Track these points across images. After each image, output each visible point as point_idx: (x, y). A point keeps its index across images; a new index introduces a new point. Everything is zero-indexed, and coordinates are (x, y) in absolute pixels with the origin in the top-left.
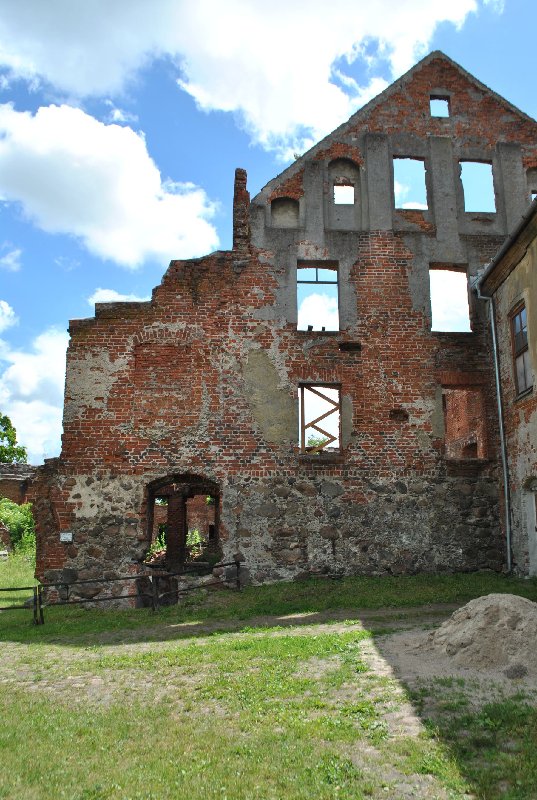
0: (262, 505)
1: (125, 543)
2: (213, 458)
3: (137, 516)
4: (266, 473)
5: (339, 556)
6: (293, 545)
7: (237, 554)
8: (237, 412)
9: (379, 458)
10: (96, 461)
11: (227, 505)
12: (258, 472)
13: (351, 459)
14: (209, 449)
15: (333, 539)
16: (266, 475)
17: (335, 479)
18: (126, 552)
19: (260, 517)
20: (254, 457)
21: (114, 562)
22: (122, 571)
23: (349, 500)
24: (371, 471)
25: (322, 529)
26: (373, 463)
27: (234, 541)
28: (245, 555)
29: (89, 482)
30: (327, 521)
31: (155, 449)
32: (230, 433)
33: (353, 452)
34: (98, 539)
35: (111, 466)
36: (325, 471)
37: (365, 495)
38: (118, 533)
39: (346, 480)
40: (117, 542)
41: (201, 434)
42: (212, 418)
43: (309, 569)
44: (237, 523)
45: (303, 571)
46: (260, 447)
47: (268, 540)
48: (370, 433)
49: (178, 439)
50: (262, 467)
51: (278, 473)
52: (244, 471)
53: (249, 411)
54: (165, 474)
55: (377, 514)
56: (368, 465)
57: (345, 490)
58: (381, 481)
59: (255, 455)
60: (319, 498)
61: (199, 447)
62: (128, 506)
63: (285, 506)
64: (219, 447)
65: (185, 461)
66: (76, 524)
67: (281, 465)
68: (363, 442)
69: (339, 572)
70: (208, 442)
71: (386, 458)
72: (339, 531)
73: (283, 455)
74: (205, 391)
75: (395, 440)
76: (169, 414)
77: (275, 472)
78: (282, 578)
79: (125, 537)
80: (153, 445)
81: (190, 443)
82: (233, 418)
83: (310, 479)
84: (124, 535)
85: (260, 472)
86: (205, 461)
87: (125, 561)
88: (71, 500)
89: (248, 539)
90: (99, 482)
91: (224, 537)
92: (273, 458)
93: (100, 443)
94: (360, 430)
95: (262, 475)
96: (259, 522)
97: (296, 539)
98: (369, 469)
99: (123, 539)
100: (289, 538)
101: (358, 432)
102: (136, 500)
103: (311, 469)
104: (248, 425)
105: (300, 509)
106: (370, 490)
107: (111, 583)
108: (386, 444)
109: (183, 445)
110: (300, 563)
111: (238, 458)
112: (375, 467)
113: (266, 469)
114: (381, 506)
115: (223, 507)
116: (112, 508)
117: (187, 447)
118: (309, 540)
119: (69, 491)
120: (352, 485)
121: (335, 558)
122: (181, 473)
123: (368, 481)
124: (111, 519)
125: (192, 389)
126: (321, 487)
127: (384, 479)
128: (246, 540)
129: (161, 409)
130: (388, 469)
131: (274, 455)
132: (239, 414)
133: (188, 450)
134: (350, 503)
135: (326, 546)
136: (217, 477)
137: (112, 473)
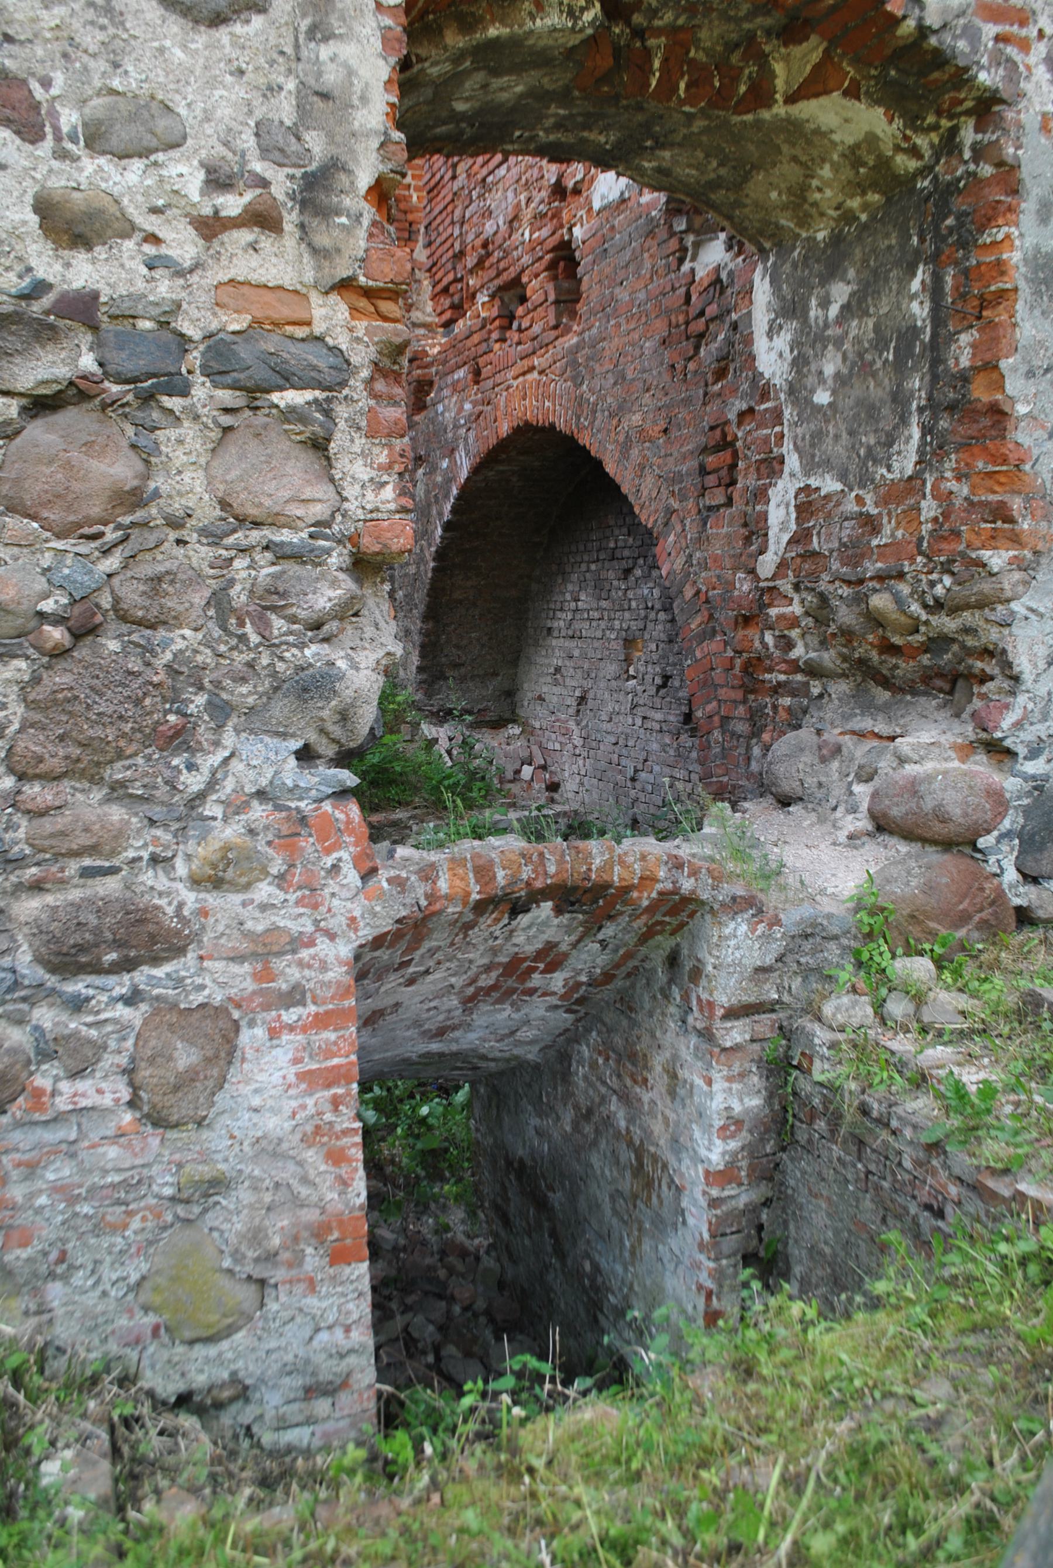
1: (219, 600)
3: (330, 315)
18: (244, 693)
21: (118, 791)
22: (213, 880)
40: (132, 594)
62: (232, 204)
79: (213, 536)
84: (208, 513)
87: (242, 776)
91: (1015, 540)
99: (201, 554)
102: (316, 143)
107: (105, 992)
115: (1025, 290)
124: (44, 333)
136: (990, 30)
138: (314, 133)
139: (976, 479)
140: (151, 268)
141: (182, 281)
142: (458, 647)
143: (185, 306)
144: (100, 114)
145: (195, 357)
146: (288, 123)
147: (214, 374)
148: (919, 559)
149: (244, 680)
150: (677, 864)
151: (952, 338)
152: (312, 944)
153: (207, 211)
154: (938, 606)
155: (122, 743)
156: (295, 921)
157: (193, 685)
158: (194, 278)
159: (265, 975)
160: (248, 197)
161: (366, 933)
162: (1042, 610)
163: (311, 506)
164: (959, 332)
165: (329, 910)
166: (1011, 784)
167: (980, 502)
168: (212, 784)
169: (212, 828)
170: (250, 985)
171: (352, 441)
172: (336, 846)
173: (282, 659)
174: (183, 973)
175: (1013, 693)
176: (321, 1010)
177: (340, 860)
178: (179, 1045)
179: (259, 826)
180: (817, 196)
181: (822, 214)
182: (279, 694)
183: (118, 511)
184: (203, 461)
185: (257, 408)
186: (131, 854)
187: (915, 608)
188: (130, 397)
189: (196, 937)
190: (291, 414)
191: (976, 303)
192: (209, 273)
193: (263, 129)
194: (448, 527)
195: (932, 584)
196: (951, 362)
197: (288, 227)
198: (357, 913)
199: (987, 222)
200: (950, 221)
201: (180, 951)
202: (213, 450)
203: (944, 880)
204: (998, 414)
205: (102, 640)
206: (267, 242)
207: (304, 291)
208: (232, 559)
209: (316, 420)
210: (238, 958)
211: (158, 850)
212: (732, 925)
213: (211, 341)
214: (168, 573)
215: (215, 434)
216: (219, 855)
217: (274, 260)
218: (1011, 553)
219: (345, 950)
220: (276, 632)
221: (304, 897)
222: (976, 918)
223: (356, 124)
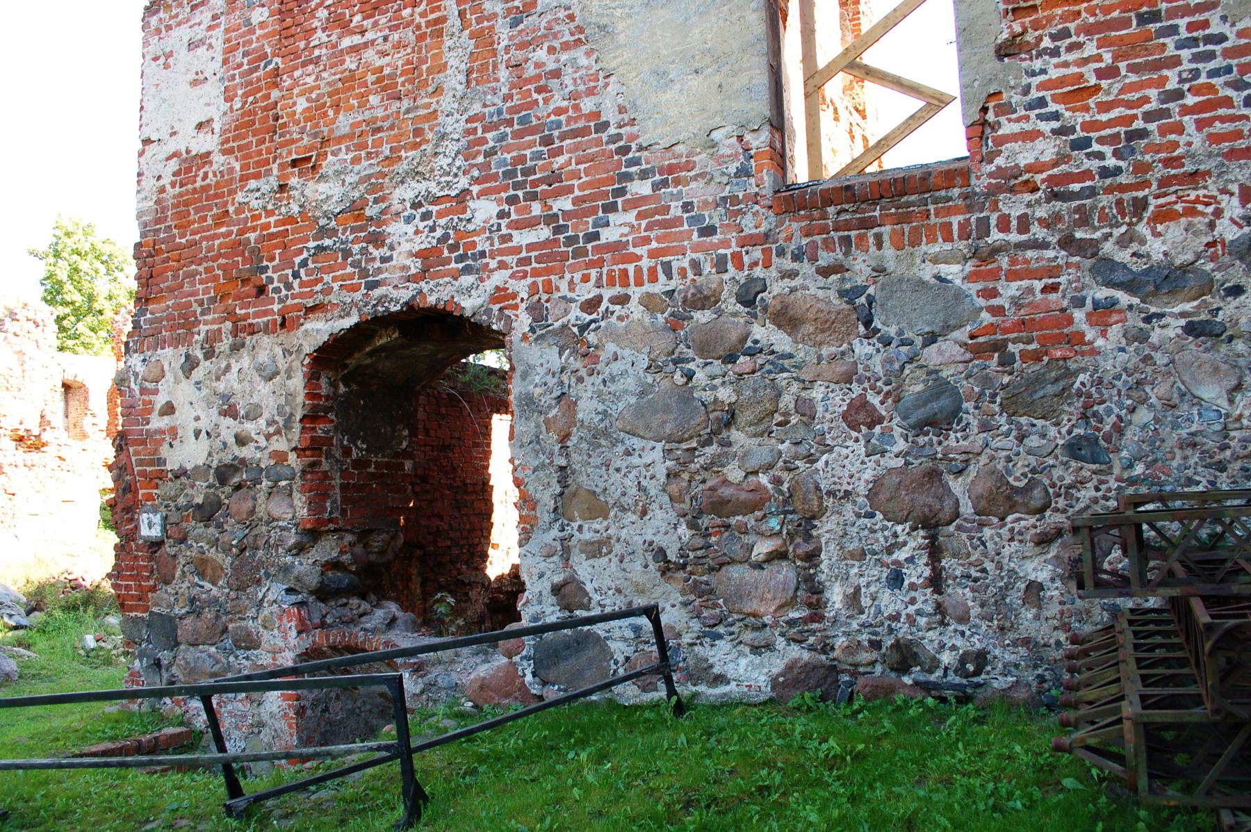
0: (642, 394)
2: (482, 244)
3: (292, 457)
4: (652, 271)
5: (960, 594)
6: (763, 548)
7: (565, 584)
8: (551, 66)
9: (1142, 134)
10: (201, 303)
12: (625, 273)
13: (1000, 161)
14: (468, 215)
15: (930, 524)
16: (653, 278)
17: (941, 263)
18: (272, 570)
19: (636, 442)
20: (612, 217)
23: (999, 347)
24: (1105, 200)
25: (877, 482)
26: (1111, 162)
27: (555, 532)
28: (589, 587)
29: (190, 365)
30: (901, 445)
31: (327, 242)
32: (531, 145)
33: (1007, 128)
34: (211, 530)
35: (231, 315)
36: (886, 230)
37: (1079, 315)
38: (252, 512)
39: (984, 256)
41: (446, 168)
42: (477, 108)
43: (826, 648)
44: (562, 468)
45: (806, 656)
46: (628, 177)
47: (666, 528)
48: (1089, 30)
49: (382, 199)
50: (638, 251)
51: (696, 265)
52: (578, 276)
53: (588, 54)
54: (353, 320)
55: (1144, 401)
56: (1087, 175)
57: (981, 302)
58: (1163, 244)
59: (611, 208)
60: (862, 348)
61: (440, 214)
63: (725, 394)
64: (499, 202)
65: (405, 268)
66: (168, 488)
67: (709, 231)
68: (1054, 74)
69: (961, 669)
70: (465, 192)
71: (1179, 129)
72: (957, 486)
73: (711, 192)
74: (454, 21)
75: (1222, 38)
76: (359, 124)
77: (685, 263)
78: (721, 679)
80: (323, 232)
81: (416, 205)
82: (539, 90)
83: (825, 272)
85: (631, 268)
86: (460, 259)
88: (157, 422)
89: (598, 524)
90: (208, 363)
92: (676, 210)
93: (210, 249)
94: (1036, 26)
95: (639, 283)
96: (635, 460)
97: (774, 523)
98: (1092, 192)
100: (750, 520)
101: (1030, 37)
102: (288, 409)
103: (824, 230)
104: (587, 105)
105: (787, 401)
106: (1102, 293)
108: (1175, 62)
109: (398, 214)
110: (791, 623)
111: (558, 230)
112: (1123, 179)
113: (653, 254)
114: (1160, 359)
116: (236, 436)
117: (409, 220)
118: (826, 528)
119: (152, 397)
120: (1013, 276)
121: (939, 608)
122: (393, 309)
123: (1088, 249)
125: (419, 27)
126: (871, 299)
127: (1174, 231)
128: (590, 530)
129: (341, 117)
130: (1194, 178)
131: (679, 196)
132: (556, 74)
133: (410, 229)
134: (1007, 361)
135: (901, 555)
136: (496, 307)
137: (235, 333)
161: (298, 651)
168: (264, 597)
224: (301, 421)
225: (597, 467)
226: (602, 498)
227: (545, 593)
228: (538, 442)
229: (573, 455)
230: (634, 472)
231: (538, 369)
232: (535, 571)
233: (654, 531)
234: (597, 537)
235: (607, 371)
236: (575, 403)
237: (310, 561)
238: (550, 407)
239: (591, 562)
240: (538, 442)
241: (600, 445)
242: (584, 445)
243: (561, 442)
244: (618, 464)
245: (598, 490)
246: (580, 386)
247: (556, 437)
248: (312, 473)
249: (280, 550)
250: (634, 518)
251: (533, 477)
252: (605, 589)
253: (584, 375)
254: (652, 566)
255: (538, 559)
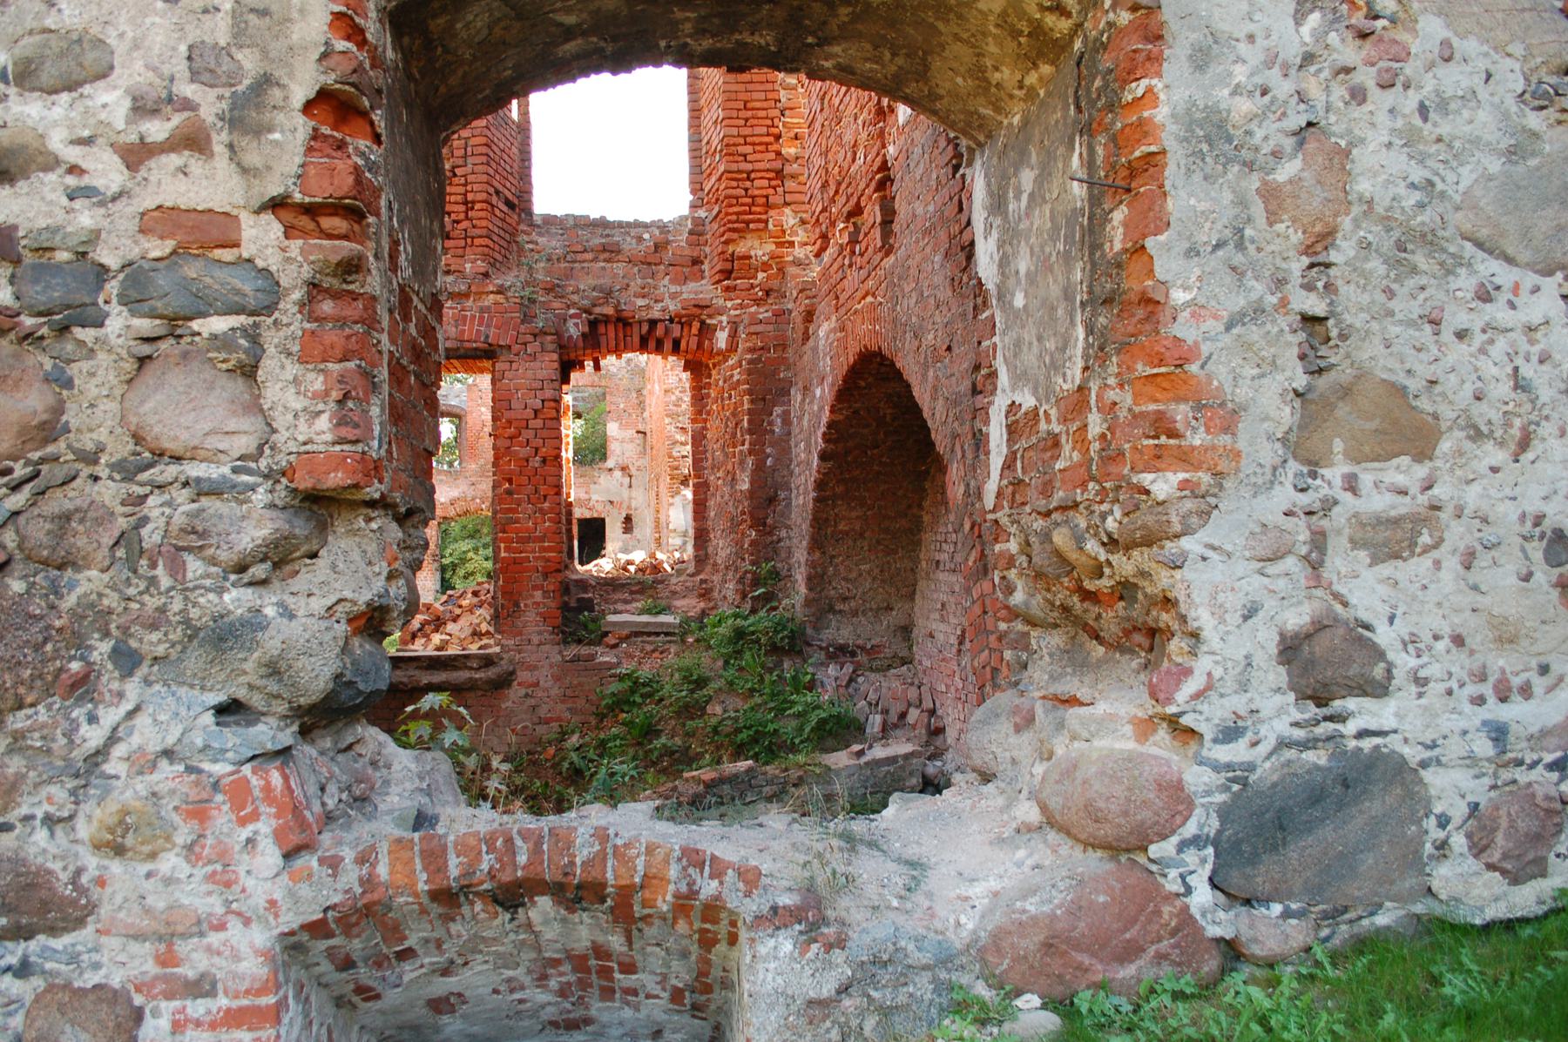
0: (1513, 154)
1: (128, 539)
3: (262, 238)
7: (1320, 626)
11: (1214, 134)
18: (152, 642)
19: (1505, 275)
27: (1284, 495)
28: (1384, 636)
38: (49, 429)
44: (1309, 320)
62: (157, 130)
79: (127, 471)
87: (146, 735)
89: (1404, 472)
91: (1185, 458)
96: (1497, 312)
99: (109, 492)
128: (1387, 487)
138: (247, 51)
139: (1138, 385)
140: (71, 199)
141: (102, 211)
142: (846, 579)
143: (103, 235)
144: (28, 53)
145: (113, 287)
146: (222, 43)
147: (133, 301)
148: (1091, 485)
149: (154, 627)
150: (693, 858)
151: (1106, 219)
152: (221, 927)
153: (133, 138)
154: (1112, 543)
155: (22, 690)
156: (199, 898)
157: (98, 630)
158: (119, 205)
159: (167, 959)
160: (177, 119)
161: (290, 920)
162: (1228, 547)
163: (235, 438)
164: (1111, 211)
165: (243, 891)
166: (1197, 778)
167: (1141, 413)
168: (113, 739)
169: (113, 789)
170: (151, 968)
171: (283, 367)
172: (255, 816)
173: (195, 604)
174: (79, 948)
175: (1193, 654)
176: (235, 1004)
177: (256, 833)
178: (68, 1028)
179: (162, 788)
180: (997, 75)
181: (1011, 97)
182: (195, 642)
183: (28, 446)
184: (118, 392)
185: (180, 336)
186: (24, 810)
187: (1092, 546)
188: (44, 331)
189: (92, 908)
190: (220, 342)
191: (1126, 173)
192: (135, 201)
193: (196, 52)
194: (823, 456)
195: (1103, 516)
196: (1107, 246)
197: (219, 148)
198: (277, 896)
199: (1131, 74)
200: (1098, 83)
201: (80, 922)
202: (130, 381)
203: (1101, 899)
204: (1151, 304)
205: (9, 580)
206: (196, 165)
207: (235, 212)
208: (146, 496)
209: (240, 346)
210: (139, 937)
211: (52, 809)
212: (772, 943)
213: (127, 270)
214: (77, 510)
215: (129, 366)
216: (116, 819)
217: (205, 183)
218: (1181, 476)
219: (261, 937)
220: (190, 575)
221: (214, 873)
222: (1152, 950)
223: (295, 37)
224: (308, 107)
225: (1410, 323)
226: (1424, 404)
227: (1259, 659)
228: (1240, 246)
229: (1343, 289)
230: (1501, 346)
231: (1243, 48)
232: (1234, 602)
233: (1544, 491)
234: (1403, 506)
235: (1429, 85)
236: (1347, 153)
237: (318, 604)
238: (1277, 154)
239: (1386, 569)
240: (1240, 246)
241: (1414, 270)
242: (1376, 265)
243: (1308, 250)
244: (1461, 319)
245: (1413, 385)
246: (1357, 112)
247: (1296, 237)
248: (336, 295)
249: (194, 567)
250: (1499, 456)
251: (1227, 339)
252: (1427, 637)
253: (1371, 84)
254: (1539, 577)
255: (1241, 567)
